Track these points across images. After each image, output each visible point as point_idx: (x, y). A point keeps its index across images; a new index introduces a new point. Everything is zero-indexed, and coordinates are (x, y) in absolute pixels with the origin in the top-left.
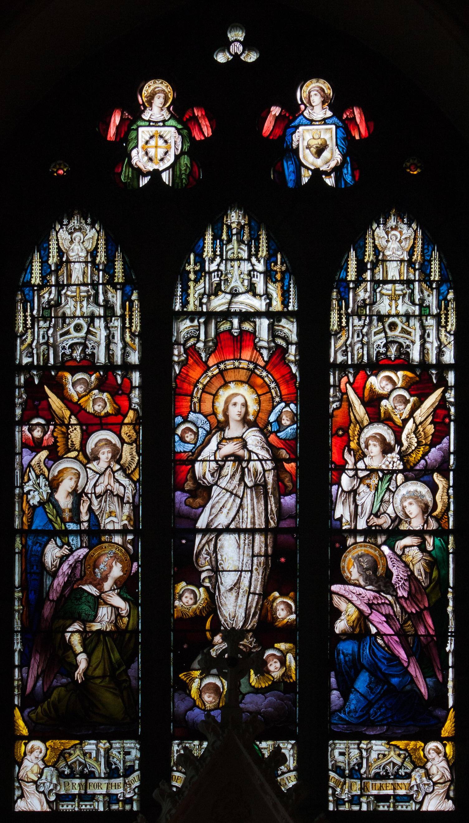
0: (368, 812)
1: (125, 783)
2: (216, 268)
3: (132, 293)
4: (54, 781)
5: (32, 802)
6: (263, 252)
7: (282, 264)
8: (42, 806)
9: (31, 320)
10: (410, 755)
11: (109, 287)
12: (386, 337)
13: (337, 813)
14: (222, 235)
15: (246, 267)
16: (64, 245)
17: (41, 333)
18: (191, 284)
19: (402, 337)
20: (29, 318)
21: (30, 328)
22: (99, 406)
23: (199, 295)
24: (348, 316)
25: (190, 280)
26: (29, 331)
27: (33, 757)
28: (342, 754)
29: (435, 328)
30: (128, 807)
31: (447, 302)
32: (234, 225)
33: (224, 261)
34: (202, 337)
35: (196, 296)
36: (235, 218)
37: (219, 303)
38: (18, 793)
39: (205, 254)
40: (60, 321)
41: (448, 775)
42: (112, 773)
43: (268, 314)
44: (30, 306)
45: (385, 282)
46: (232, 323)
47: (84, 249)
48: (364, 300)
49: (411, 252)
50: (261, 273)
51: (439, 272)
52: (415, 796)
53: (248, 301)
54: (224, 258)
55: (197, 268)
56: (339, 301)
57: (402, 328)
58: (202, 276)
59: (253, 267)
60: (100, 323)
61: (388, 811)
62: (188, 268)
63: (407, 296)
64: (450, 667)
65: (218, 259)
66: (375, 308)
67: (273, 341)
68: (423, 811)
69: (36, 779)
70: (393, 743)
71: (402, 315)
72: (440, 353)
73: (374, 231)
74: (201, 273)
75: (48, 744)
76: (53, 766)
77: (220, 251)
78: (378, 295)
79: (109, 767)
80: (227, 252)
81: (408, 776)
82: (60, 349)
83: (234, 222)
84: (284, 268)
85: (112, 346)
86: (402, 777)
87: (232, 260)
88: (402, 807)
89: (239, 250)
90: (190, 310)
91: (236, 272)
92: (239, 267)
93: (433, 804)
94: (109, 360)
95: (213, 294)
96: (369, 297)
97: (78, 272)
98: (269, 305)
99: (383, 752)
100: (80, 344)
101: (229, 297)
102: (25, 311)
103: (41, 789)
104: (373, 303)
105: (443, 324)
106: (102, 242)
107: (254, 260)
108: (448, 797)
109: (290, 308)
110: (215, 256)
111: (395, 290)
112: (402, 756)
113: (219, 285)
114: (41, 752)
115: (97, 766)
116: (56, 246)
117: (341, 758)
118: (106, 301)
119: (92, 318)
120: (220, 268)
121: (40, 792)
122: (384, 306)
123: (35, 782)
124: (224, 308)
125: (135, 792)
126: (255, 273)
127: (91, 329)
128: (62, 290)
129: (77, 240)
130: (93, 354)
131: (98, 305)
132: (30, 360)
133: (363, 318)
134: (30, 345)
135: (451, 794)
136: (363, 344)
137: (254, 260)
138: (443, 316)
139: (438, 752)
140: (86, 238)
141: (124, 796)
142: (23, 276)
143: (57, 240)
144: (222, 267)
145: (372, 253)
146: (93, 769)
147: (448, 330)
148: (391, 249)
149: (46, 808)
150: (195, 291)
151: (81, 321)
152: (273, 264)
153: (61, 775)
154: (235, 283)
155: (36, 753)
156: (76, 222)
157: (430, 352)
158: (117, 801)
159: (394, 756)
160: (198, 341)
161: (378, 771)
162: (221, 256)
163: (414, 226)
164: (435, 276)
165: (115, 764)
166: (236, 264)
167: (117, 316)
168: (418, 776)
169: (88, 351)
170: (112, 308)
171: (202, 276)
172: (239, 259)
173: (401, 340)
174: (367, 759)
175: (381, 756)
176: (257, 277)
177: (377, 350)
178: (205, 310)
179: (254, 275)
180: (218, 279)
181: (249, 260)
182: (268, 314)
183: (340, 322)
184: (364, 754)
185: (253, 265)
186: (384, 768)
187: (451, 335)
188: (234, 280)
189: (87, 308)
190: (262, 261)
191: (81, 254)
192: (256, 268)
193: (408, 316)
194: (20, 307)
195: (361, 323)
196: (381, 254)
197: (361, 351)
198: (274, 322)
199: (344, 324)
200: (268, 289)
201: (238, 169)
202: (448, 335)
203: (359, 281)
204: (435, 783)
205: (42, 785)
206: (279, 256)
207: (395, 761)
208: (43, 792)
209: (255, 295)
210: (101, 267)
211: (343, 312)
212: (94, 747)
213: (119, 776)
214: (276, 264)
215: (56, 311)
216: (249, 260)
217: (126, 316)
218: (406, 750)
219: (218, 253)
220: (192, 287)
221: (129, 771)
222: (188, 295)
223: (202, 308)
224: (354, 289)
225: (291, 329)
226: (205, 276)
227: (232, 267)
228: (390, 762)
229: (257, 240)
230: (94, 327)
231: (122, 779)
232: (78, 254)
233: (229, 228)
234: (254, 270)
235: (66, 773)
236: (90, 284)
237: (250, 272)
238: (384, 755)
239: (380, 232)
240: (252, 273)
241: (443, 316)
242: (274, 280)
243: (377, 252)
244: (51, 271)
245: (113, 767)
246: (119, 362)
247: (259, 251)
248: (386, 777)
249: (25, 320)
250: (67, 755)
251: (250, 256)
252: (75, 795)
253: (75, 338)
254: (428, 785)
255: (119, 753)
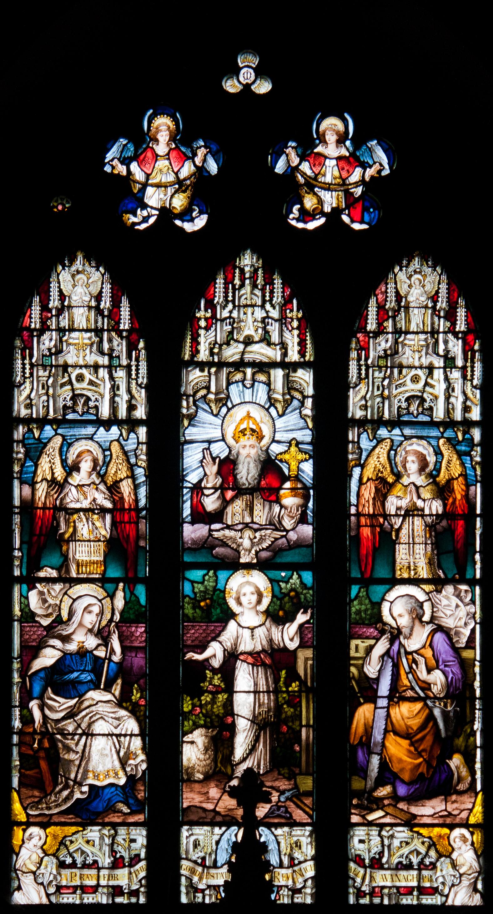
0: (389, 905)
1: (130, 873)
2: (228, 315)
3: (475, 343)
4: (54, 872)
5: (29, 894)
6: (278, 298)
7: (298, 311)
8: (41, 898)
9: (365, 370)
10: (434, 844)
11: (450, 335)
12: (73, 390)
13: (191, 905)
14: (234, 280)
15: (259, 314)
16: (66, 288)
17: (376, 384)
18: (202, 332)
19: (90, 390)
20: (28, 367)
21: (29, 378)
22: (86, 461)
23: (210, 344)
24: (32, 366)
25: (200, 327)
26: (28, 381)
27: (30, 846)
28: (361, 841)
29: (125, 379)
30: (134, 900)
31: (474, 352)
32: (247, 269)
33: (237, 308)
34: (213, 389)
35: (207, 344)
36: (247, 261)
37: (232, 353)
38: (16, 884)
39: (216, 300)
40: (396, 371)
41: (475, 865)
42: (117, 863)
43: (283, 365)
44: (29, 353)
45: (72, 330)
46: (245, 374)
47: (87, 292)
48: (385, 351)
49: (434, 298)
50: (276, 321)
51: (465, 320)
52: (440, 888)
53: (262, 351)
54: (237, 304)
55: (209, 315)
56: (23, 350)
57: (90, 380)
58: (213, 323)
59: (267, 314)
60: (438, 374)
61: (412, 905)
62: (198, 315)
63: (95, 346)
64: (16, 745)
65: (230, 306)
66: (397, 360)
67: (289, 394)
68: (449, 906)
69: (34, 869)
70: (415, 829)
71: (91, 366)
72: (131, 408)
73: (395, 275)
74: (212, 321)
75: (48, 831)
76: (54, 855)
77: (269, 296)
78: (64, 344)
79: (112, 857)
80: (240, 298)
81: (433, 866)
82: (61, 400)
83: (247, 265)
84: (300, 315)
85: (452, 400)
86: (426, 868)
87: (246, 306)
88: (427, 900)
89: (253, 296)
90: (200, 360)
91: (250, 320)
92: (253, 314)
93: (461, 897)
94: (448, 415)
95: (224, 344)
96: (390, 347)
97: (417, 319)
98: (285, 354)
99: (406, 840)
100: (417, 397)
101: (241, 347)
102: (23, 358)
103: (40, 881)
104: (59, 351)
105: (469, 377)
106: (444, 287)
107: (268, 306)
108: (475, 890)
109: (307, 358)
110: (227, 302)
111: (419, 340)
112: (426, 844)
113: (231, 333)
114: (40, 839)
115: (101, 856)
116: (57, 289)
117: (361, 846)
118: (447, 351)
119: (431, 369)
120: (233, 315)
121: (38, 884)
122: (71, 356)
123: (34, 873)
124: (237, 357)
125: (141, 883)
126: (270, 320)
127: (429, 380)
128: (400, 337)
129: (80, 283)
130: (96, 407)
131: (102, 353)
132: (364, 413)
133: (48, 368)
134: (364, 397)
135: (480, 886)
136: (384, 398)
137: (268, 306)
138: (469, 369)
139: (464, 839)
140: (90, 281)
141: (129, 887)
142: (21, 320)
143: (59, 283)
144: (235, 314)
145: (394, 299)
146: (96, 858)
147: (139, 383)
148: (415, 295)
149: (45, 901)
150: (205, 341)
151: (419, 372)
152: (288, 311)
153: (62, 865)
154: (249, 329)
155: (35, 841)
156: (416, 264)
157: (120, 406)
158: (122, 894)
159: (82, 843)
160: (209, 392)
161: (401, 859)
162: (233, 301)
163: (438, 269)
164: (125, 325)
165: (120, 852)
166: (250, 310)
167: (458, 368)
168: (444, 866)
169: (426, 405)
170: (453, 359)
171: (213, 323)
172: (253, 306)
173: (89, 394)
174: (389, 846)
175: (404, 844)
176: (272, 325)
177: (399, 404)
178: (216, 360)
179: (268, 322)
180: (230, 327)
181: (263, 306)
182: (283, 365)
183: (360, 373)
184: (386, 842)
185: (267, 312)
186: (407, 857)
187: (142, 388)
188: (247, 328)
189: (92, 358)
190: (277, 308)
191: (84, 298)
192: (270, 315)
193: (96, 367)
194: (354, 355)
195: (382, 375)
196: (404, 300)
197: (381, 405)
198: (289, 372)
199: (363, 376)
200: (284, 338)
201: (246, 207)
202: (138, 388)
203: (44, 328)
204: (461, 875)
205: (41, 876)
206: (295, 301)
207: (418, 849)
208: (42, 884)
209: (269, 344)
210: (442, 314)
211: (362, 362)
212: (97, 834)
213: (124, 866)
214: (292, 311)
215: (56, 360)
216: (263, 306)
217: (131, 366)
218: (430, 838)
219: (230, 298)
220: (202, 336)
221: (135, 859)
222: (199, 343)
223: (213, 359)
224: (39, 337)
225: (307, 380)
226: (216, 324)
227: (245, 314)
228: (77, 850)
229: (272, 284)
230: (432, 378)
231: (127, 869)
232: (81, 298)
233: (242, 271)
234: (268, 317)
235: (67, 863)
236: (430, 333)
237: (263, 320)
238: (407, 843)
239: (402, 276)
240: (267, 320)
241: (469, 369)
242: (290, 328)
243: (399, 298)
244: (52, 316)
245: (118, 856)
246: (459, 419)
247: (274, 297)
248: (409, 867)
249: (24, 368)
250: (68, 843)
251: (264, 302)
252: (412, 888)
253: (413, 390)
254: (454, 876)
255: (124, 840)
